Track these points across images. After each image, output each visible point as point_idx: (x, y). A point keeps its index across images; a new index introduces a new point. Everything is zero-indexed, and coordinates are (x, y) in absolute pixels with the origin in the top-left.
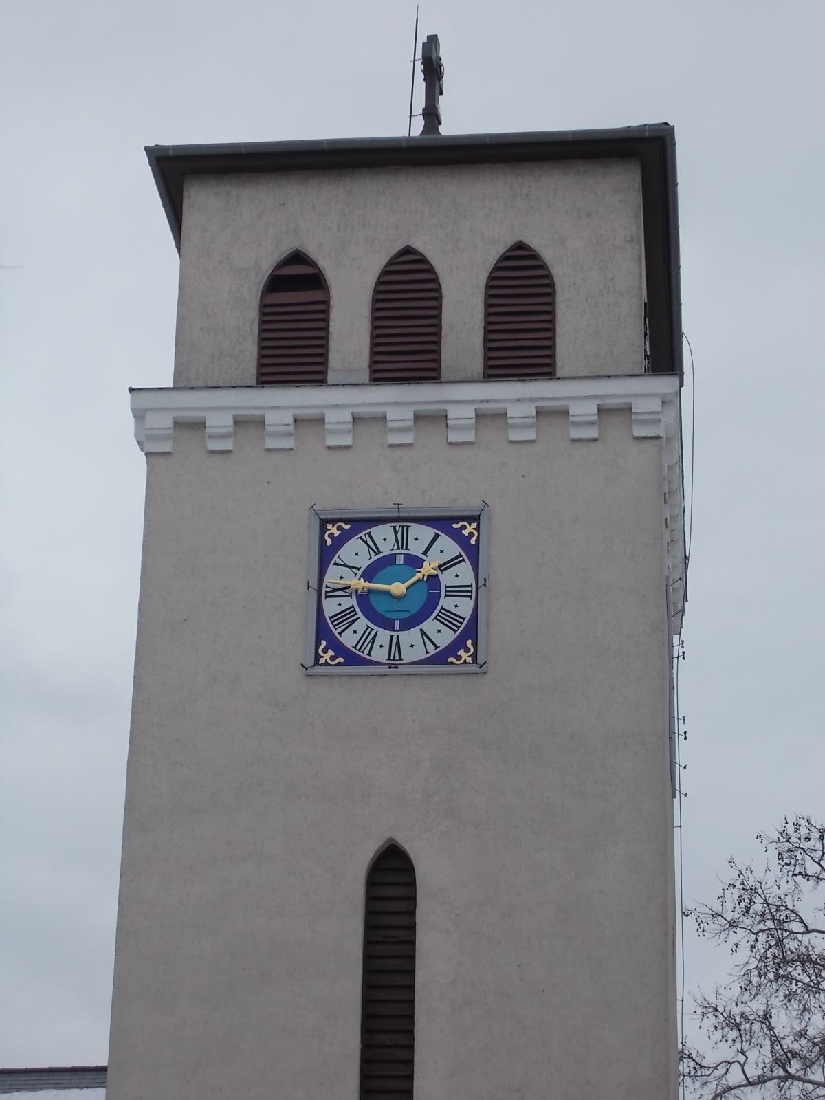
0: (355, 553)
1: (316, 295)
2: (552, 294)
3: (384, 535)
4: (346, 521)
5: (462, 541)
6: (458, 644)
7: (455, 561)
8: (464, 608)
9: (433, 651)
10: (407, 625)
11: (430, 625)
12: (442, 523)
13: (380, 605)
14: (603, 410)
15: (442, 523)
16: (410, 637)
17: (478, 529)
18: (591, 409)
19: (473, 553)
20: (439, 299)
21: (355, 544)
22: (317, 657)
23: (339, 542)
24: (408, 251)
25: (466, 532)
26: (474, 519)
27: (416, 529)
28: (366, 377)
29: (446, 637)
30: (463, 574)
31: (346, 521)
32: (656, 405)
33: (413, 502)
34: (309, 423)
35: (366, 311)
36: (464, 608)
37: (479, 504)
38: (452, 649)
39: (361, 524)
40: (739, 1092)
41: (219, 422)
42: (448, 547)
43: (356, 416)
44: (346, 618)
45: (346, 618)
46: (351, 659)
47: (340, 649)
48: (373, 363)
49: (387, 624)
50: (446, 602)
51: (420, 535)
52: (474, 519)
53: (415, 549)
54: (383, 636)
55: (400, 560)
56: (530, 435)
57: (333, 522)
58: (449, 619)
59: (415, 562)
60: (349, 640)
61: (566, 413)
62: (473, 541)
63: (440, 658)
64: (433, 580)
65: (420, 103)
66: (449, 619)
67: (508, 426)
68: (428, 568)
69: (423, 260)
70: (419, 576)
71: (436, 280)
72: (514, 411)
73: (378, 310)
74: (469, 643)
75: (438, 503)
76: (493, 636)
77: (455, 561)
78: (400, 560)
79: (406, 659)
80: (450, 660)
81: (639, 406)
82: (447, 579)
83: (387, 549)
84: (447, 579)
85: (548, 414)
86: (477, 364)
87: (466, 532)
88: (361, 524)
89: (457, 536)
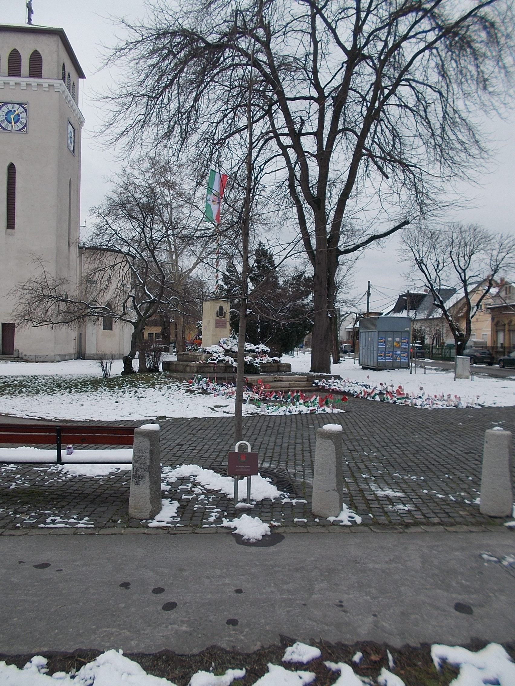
2: (42, 61)
5: (24, 108)
6: (23, 128)
7: (22, 112)
8: (24, 121)
12: (20, 104)
13: (16, 120)
15: (20, 104)
20: (21, 60)
21: (4, 107)
24: (15, 49)
27: (16, 105)
28: (7, 74)
29: (21, 126)
30: (24, 115)
32: (58, 85)
33: (14, 100)
34: (17, 84)
35: (29, 61)
36: (24, 121)
39: (6, 103)
40: (485, 301)
42: (22, 109)
48: (9, 72)
50: (21, 120)
51: (17, 106)
56: (36, 89)
58: (22, 123)
61: (42, 85)
63: (20, 130)
65: (27, 16)
66: (22, 123)
68: (17, 112)
69: (18, 52)
71: (20, 56)
72: (33, 84)
75: (20, 101)
76: (30, 127)
77: (22, 112)
81: (55, 85)
83: (10, 109)
84: (21, 115)
85: (39, 85)
86: (27, 73)
88: (6, 103)
89: (23, 107)
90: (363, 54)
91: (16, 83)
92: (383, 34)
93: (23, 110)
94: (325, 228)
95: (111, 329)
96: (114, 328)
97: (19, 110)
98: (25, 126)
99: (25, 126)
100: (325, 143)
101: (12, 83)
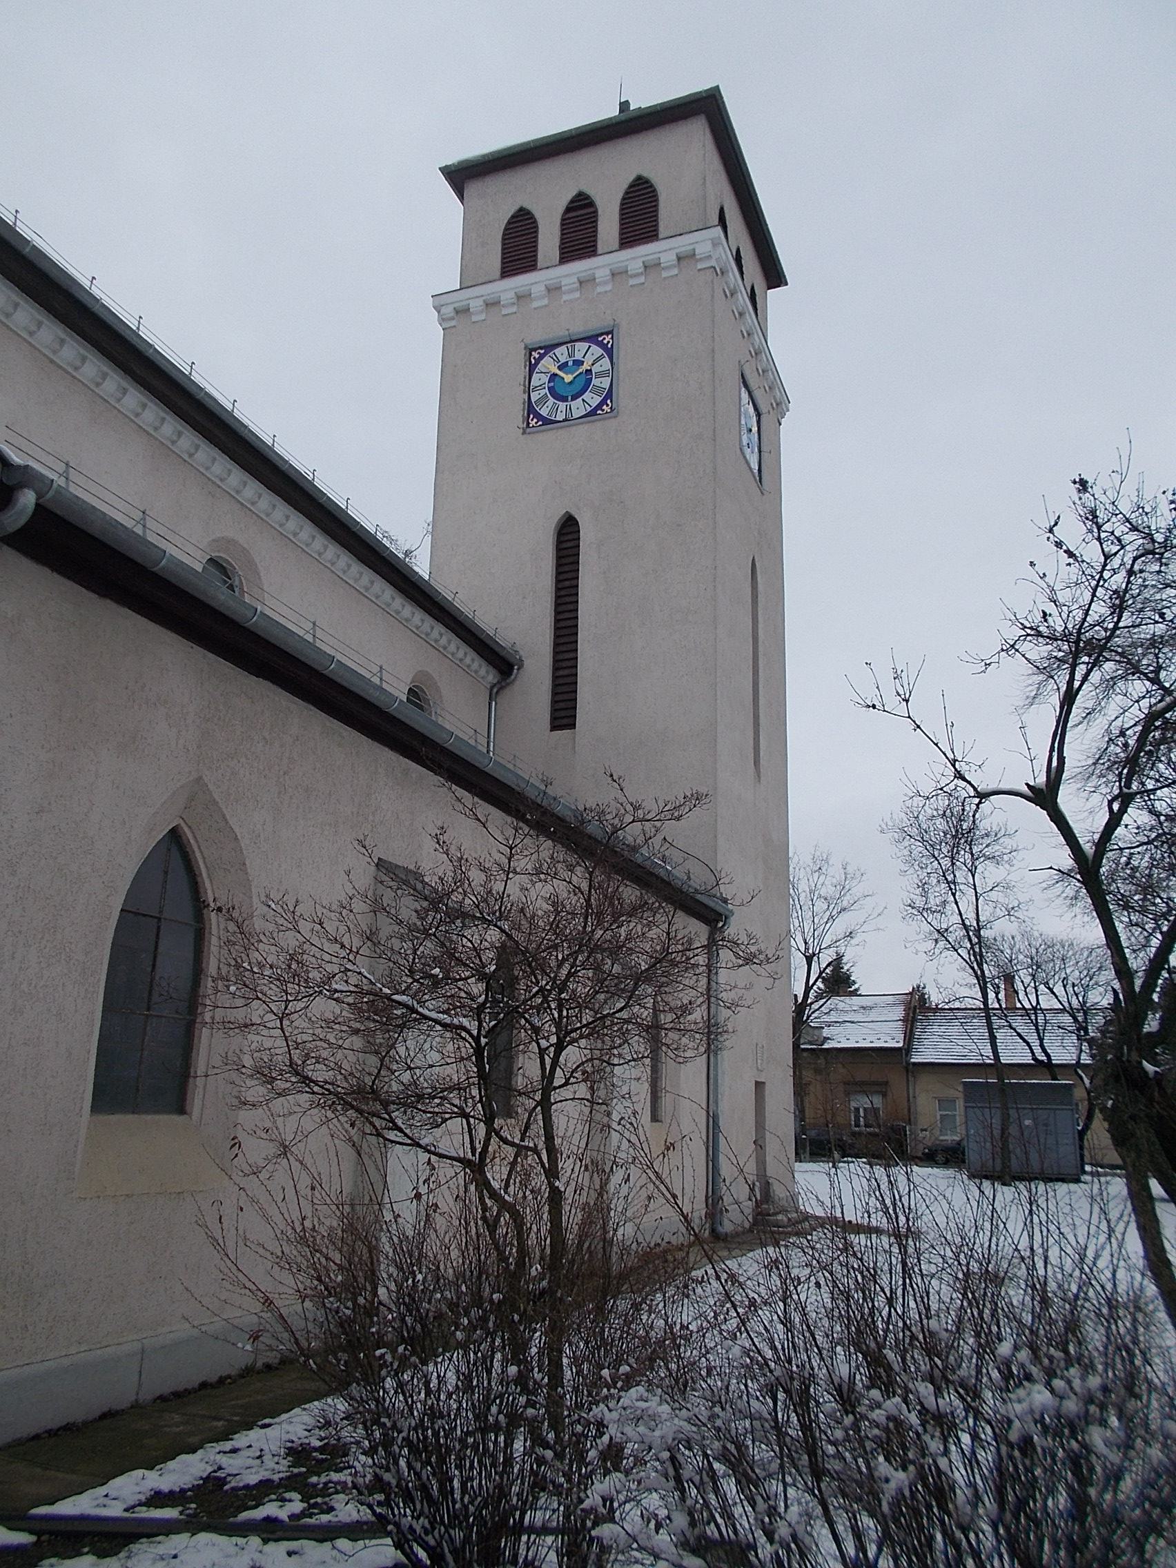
0: (548, 364)
1: (592, 210)
3: (562, 353)
4: (541, 348)
6: (603, 402)
7: (602, 356)
8: (605, 383)
9: (589, 409)
10: (574, 398)
11: (587, 396)
12: (592, 339)
14: (684, 258)
15: (592, 339)
16: (574, 404)
17: (612, 338)
18: (480, 302)
19: (609, 352)
22: (528, 423)
23: (538, 361)
25: (605, 342)
26: (611, 332)
31: (541, 348)
33: (560, 333)
34: (522, 297)
35: (617, 209)
37: (612, 323)
38: (599, 406)
39: (549, 348)
41: (476, 305)
42: (597, 351)
43: (681, 255)
44: (543, 400)
45: (543, 400)
46: (547, 421)
47: (539, 416)
49: (564, 399)
51: (581, 347)
52: (611, 332)
53: (578, 356)
54: (562, 406)
55: (570, 363)
57: (535, 350)
58: (598, 390)
59: (579, 363)
60: (544, 412)
62: (609, 346)
63: (593, 413)
64: (589, 372)
66: (598, 390)
67: (472, 314)
68: (586, 367)
70: (581, 370)
73: (655, 206)
74: (609, 402)
77: (602, 356)
78: (570, 363)
79: (575, 417)
80: (599, 412)
82: (595, 369)
84: (595, 369)
87: (605, 342)
88: (549, 348)
90: (1149, 1033)
91: (457, 312)
92: (578, 1189)
93: (600, 351)
94: (1133, 983)
95: (181, 1110)
96: (196, 1102)
97: (589, 354)
98: (609, 395)
99: (609, 395)
100: (548, 1068)
101: (538, 290)
